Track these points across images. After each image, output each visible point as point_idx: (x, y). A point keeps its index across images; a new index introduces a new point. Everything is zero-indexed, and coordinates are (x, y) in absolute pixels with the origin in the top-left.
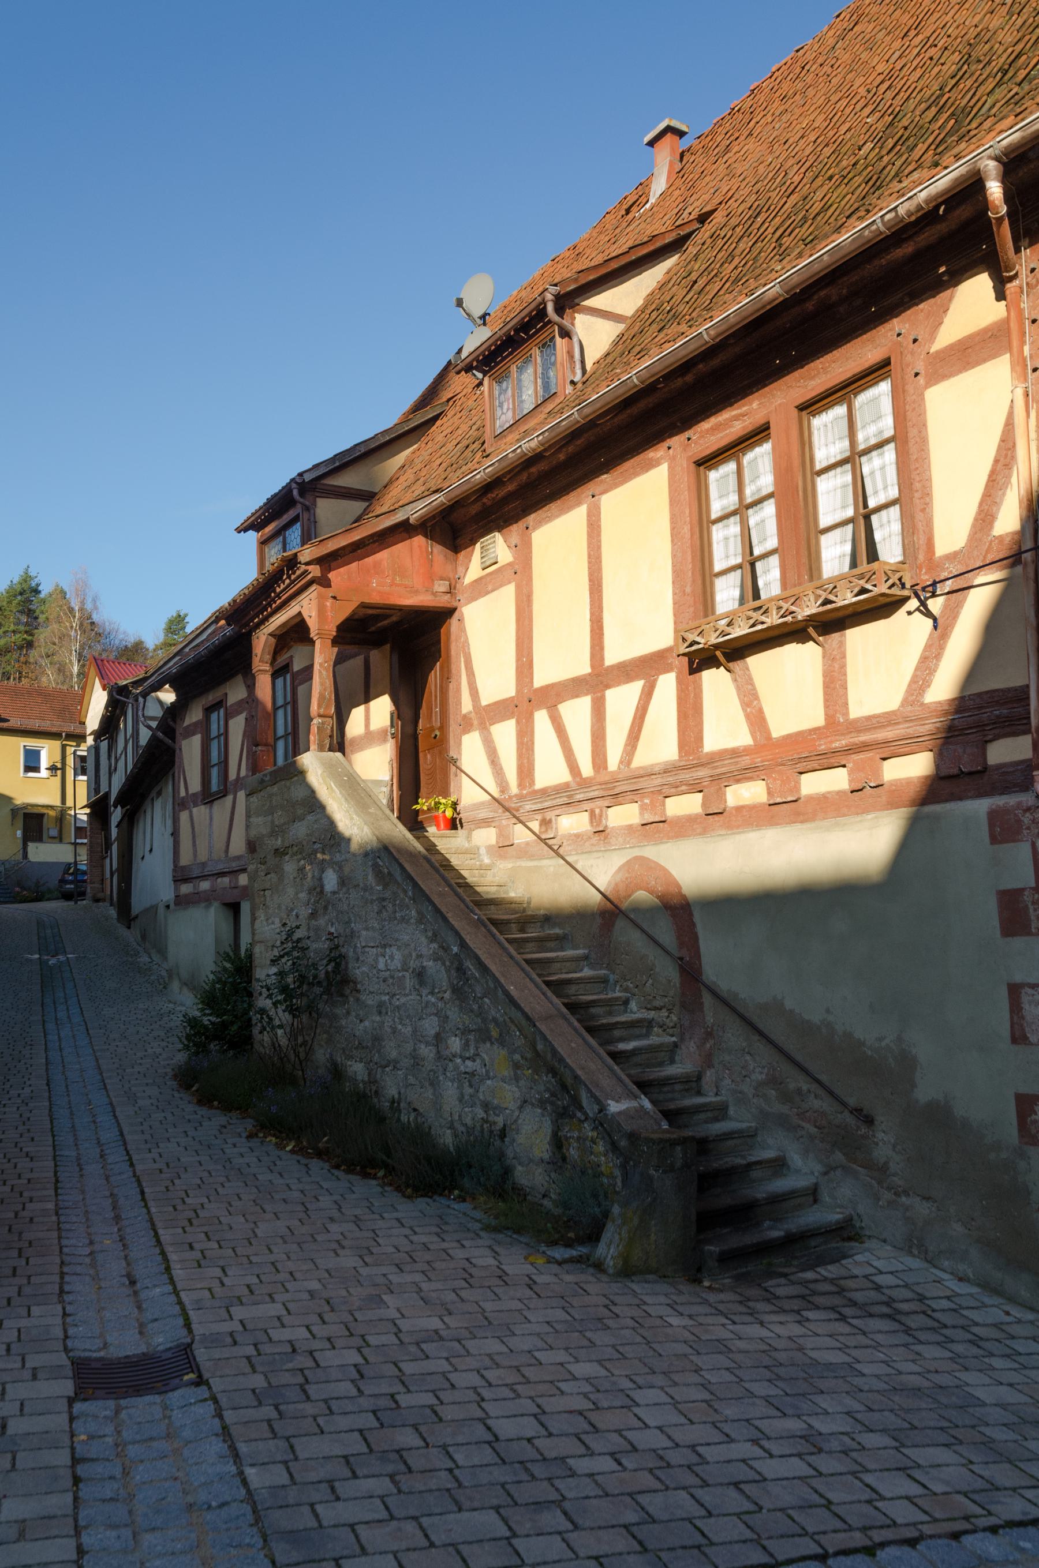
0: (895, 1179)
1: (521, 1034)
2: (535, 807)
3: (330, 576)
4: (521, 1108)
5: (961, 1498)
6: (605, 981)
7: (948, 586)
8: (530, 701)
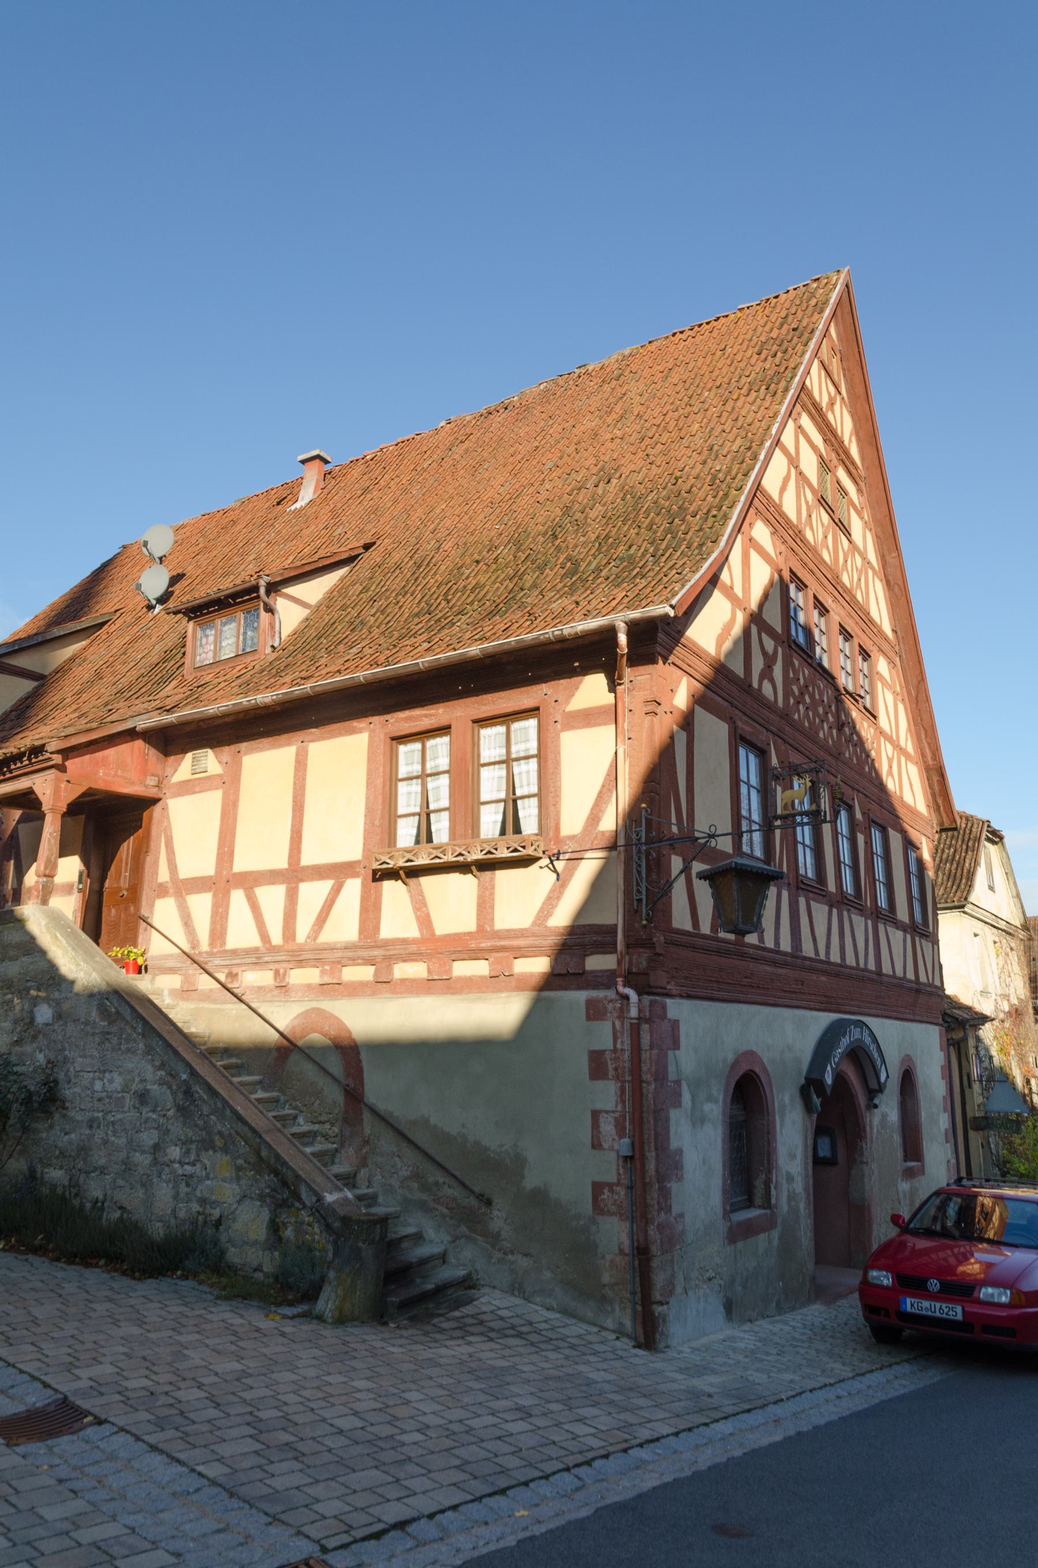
0: (505, 1243)
1: (246, 1142)
2: (223, 963)
3: (67, 763)
4: (239, 1202)
5: (616, 1432)
6: (276, 1101)
7: (567, 856)
8: (224, 882)
